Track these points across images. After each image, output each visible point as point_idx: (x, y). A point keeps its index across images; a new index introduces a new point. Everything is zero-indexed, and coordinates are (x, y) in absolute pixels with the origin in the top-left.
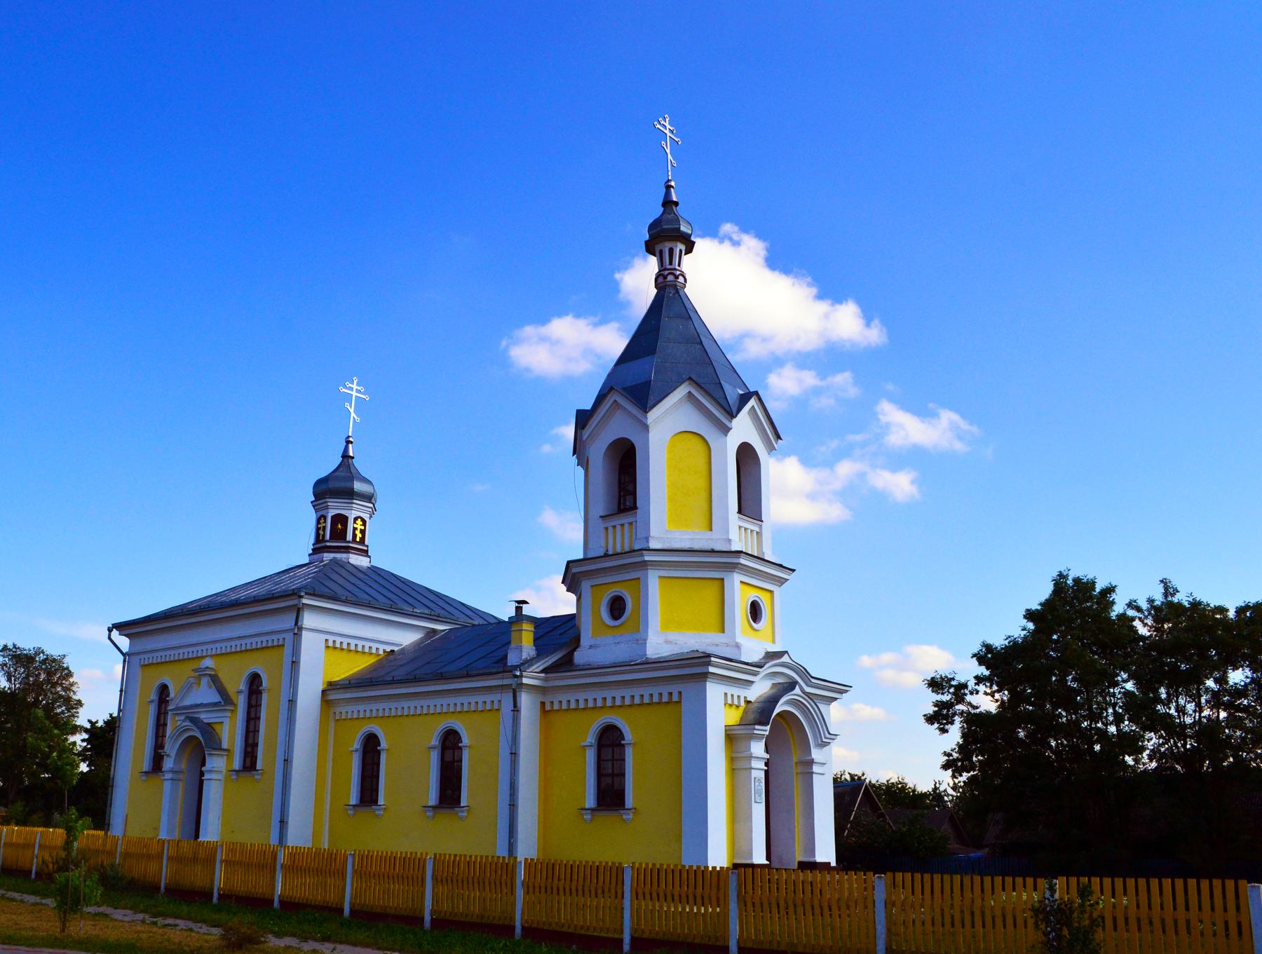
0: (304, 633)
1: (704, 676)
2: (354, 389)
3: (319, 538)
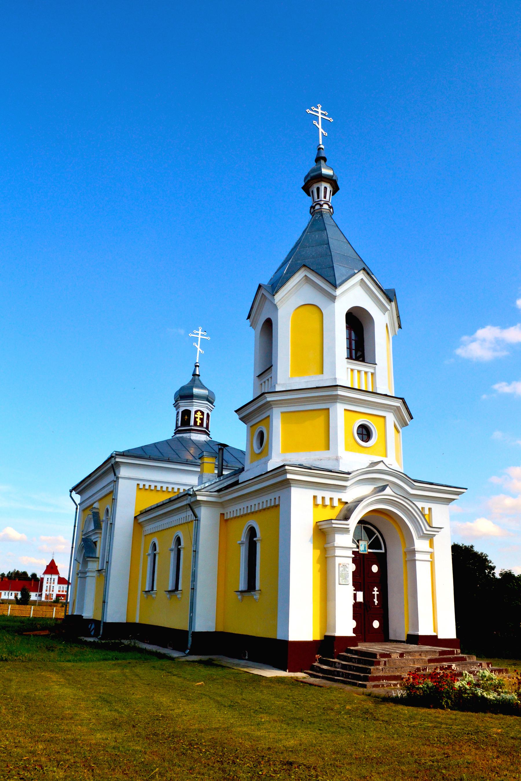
0: (120, 480)
1: (287, 484)
2: (200, 334)
3: (177, 427)
